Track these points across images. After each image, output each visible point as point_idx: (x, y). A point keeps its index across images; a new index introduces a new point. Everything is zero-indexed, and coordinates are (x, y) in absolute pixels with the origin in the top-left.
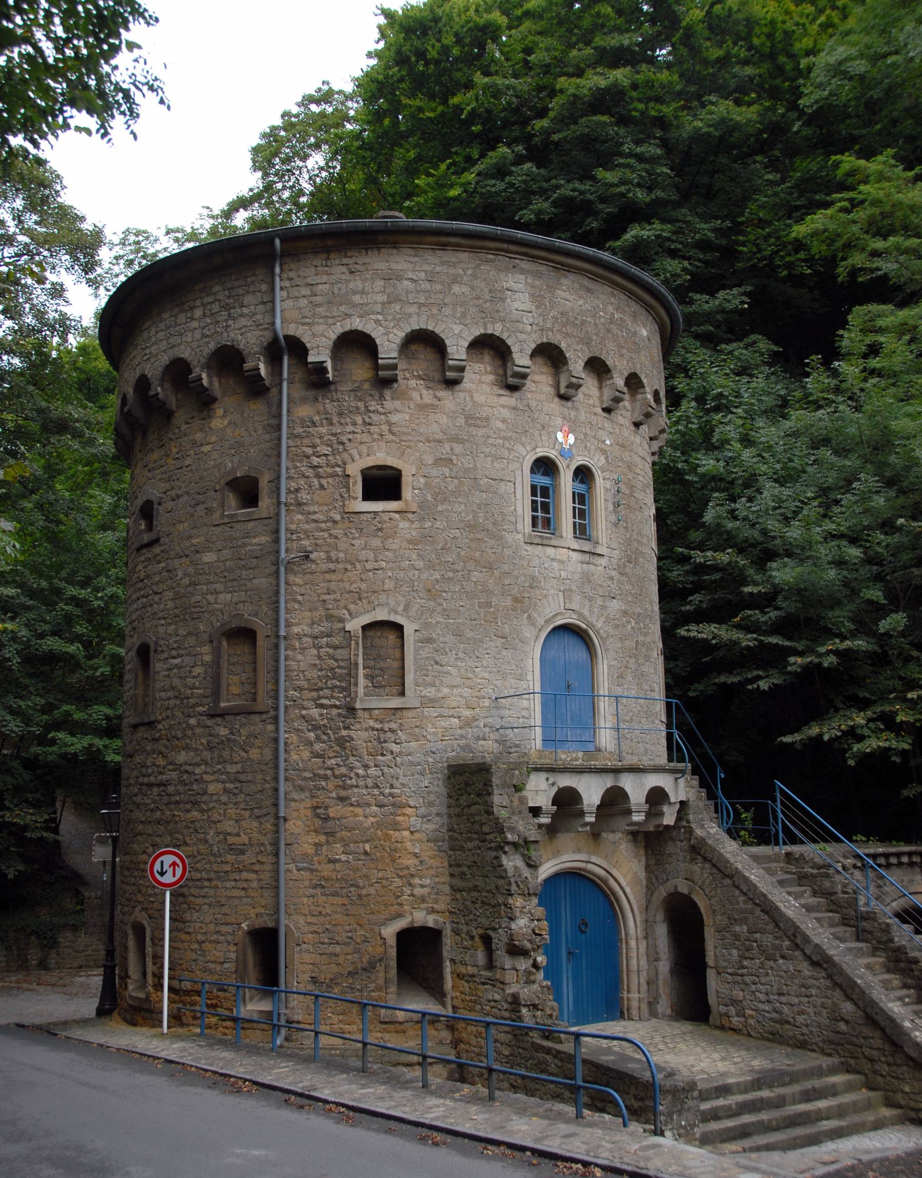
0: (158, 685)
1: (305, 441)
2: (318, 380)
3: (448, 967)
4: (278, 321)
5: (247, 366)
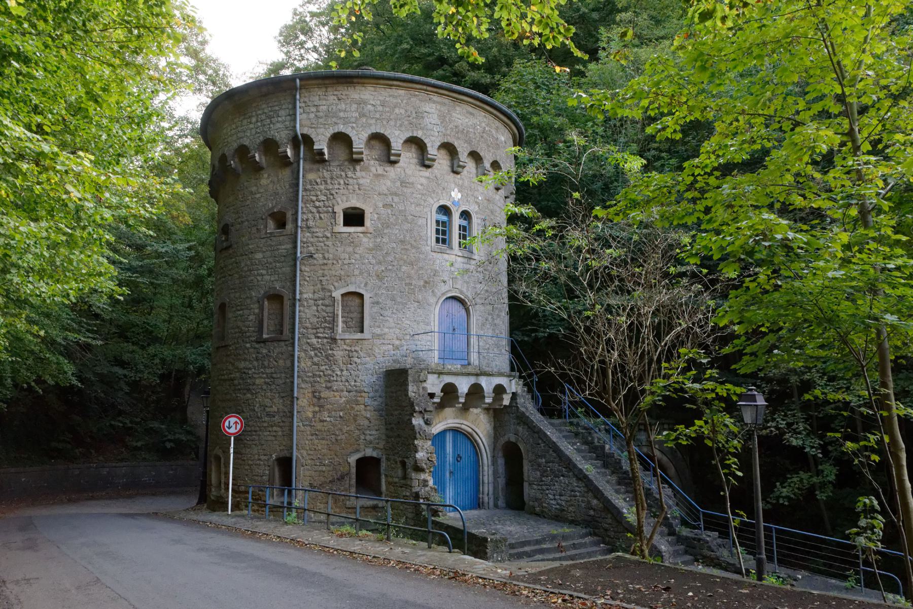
1: (313, 193)
2: (318, 158)
4: (298, 126)
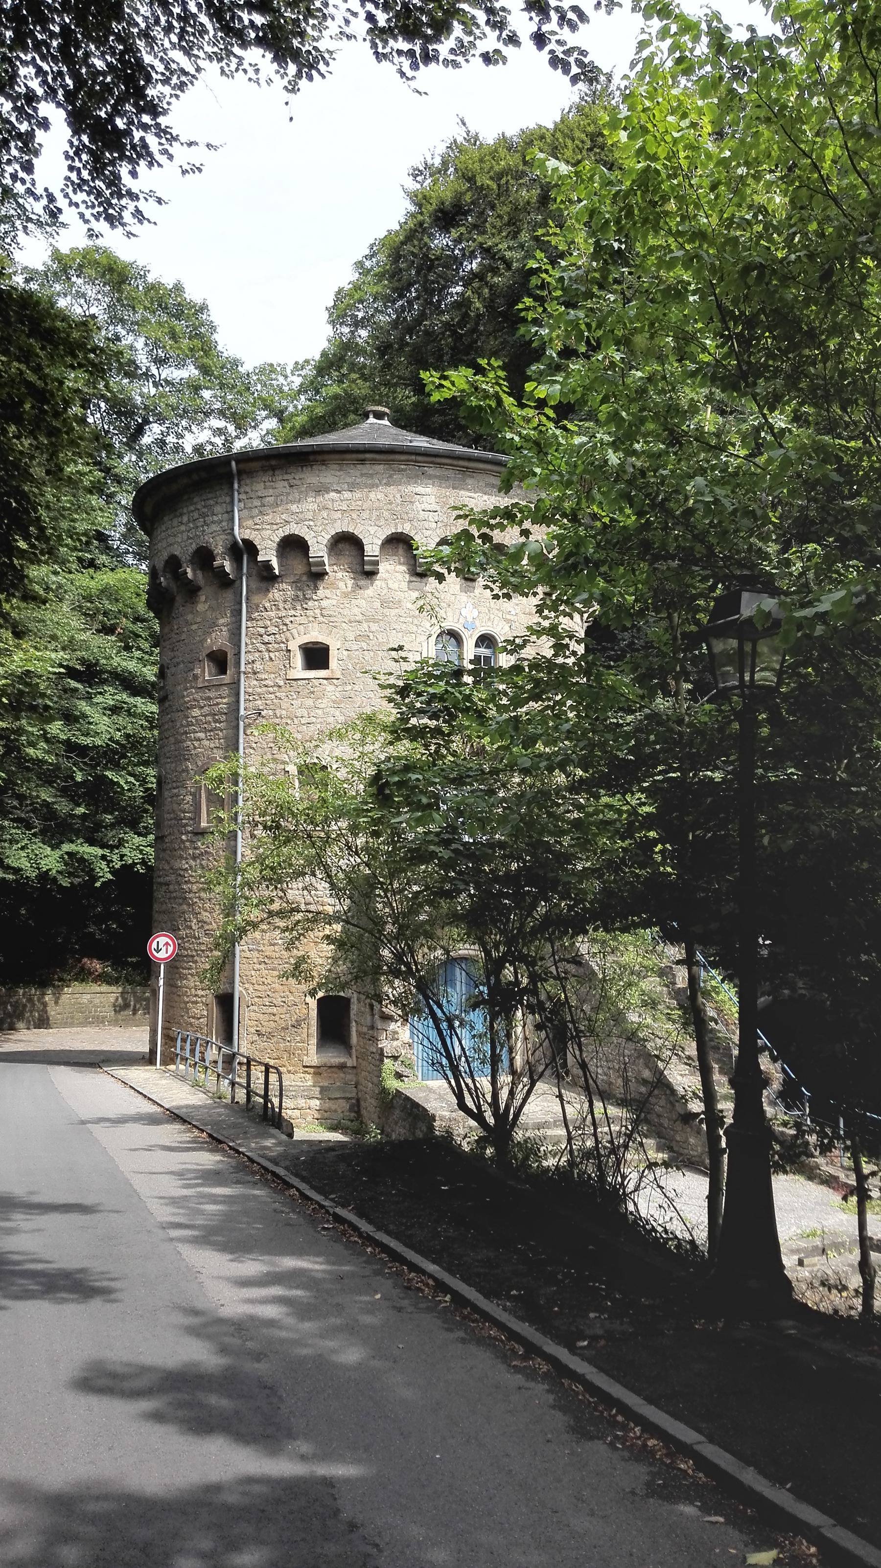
0: (166, 808)
1: (260, 623)
2: (267, 577)
3: (354, 1030)
4: (236, 528)
5: (216, 563)
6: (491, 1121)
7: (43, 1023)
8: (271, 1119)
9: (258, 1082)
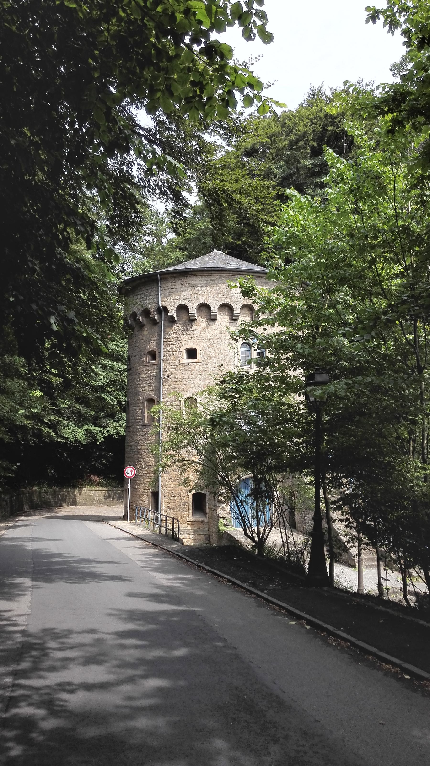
0: (131, 415)
1: (169, 340)
2: (172, 321)
3: (207, 506)
4: (160, 301)
6: (256, 539)
7: (74, 503)
8: (174, 538)
9: (170, 526)
